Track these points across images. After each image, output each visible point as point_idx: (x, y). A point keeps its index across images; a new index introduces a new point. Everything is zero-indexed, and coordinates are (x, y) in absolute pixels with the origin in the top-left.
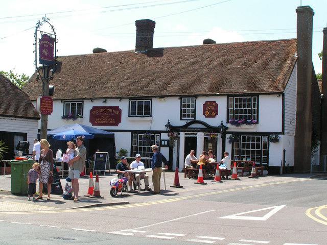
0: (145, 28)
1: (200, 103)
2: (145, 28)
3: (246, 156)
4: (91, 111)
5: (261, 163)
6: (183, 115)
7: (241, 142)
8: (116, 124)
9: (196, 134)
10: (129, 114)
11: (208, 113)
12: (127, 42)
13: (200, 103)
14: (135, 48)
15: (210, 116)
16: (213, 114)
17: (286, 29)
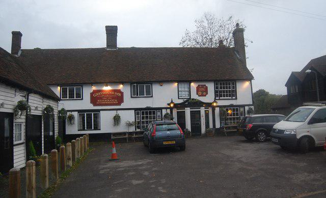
0: (112, 32)
4: (92, 94)
8: (119, 104)
11: (200, 93)
14: (105, 46)
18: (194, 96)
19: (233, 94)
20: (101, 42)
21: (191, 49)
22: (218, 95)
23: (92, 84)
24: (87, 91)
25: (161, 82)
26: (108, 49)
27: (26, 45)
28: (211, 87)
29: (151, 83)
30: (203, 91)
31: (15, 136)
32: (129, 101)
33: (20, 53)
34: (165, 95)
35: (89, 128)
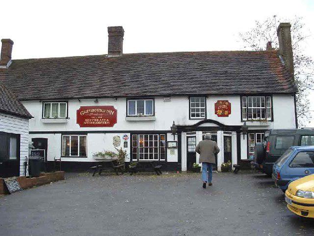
0: (116, 34)
1: (211, 104)
2: (116, 34)
3: (149, 153)
4: (78, 112)
5: (138, 160)
6: (192, 115)
7: (158, 141)
8: (111, 125)
9: (195, 133)
10: (43, 116)
11: (220, 112)
12: (100, 47)
13: (211, 104)
14: (107, 53)
15: (223, 115)
16: (226, 112)
17: (263, 39)
18: (211, 115)
19: (265, 113)
20: (100, 47)
21: (249, 52)
22: (246, 114)
23: (79, 99)
24: (73, 108)
25: (168, 96)
26: (109, 56)
27: (129, 47)
28: (235, 104)
29: (153, 97)
30: (225, 110)
31: (286, 158)
32: (122, 123)
33: (9, 63)
34: (170, 113)
35: (74, 153)
